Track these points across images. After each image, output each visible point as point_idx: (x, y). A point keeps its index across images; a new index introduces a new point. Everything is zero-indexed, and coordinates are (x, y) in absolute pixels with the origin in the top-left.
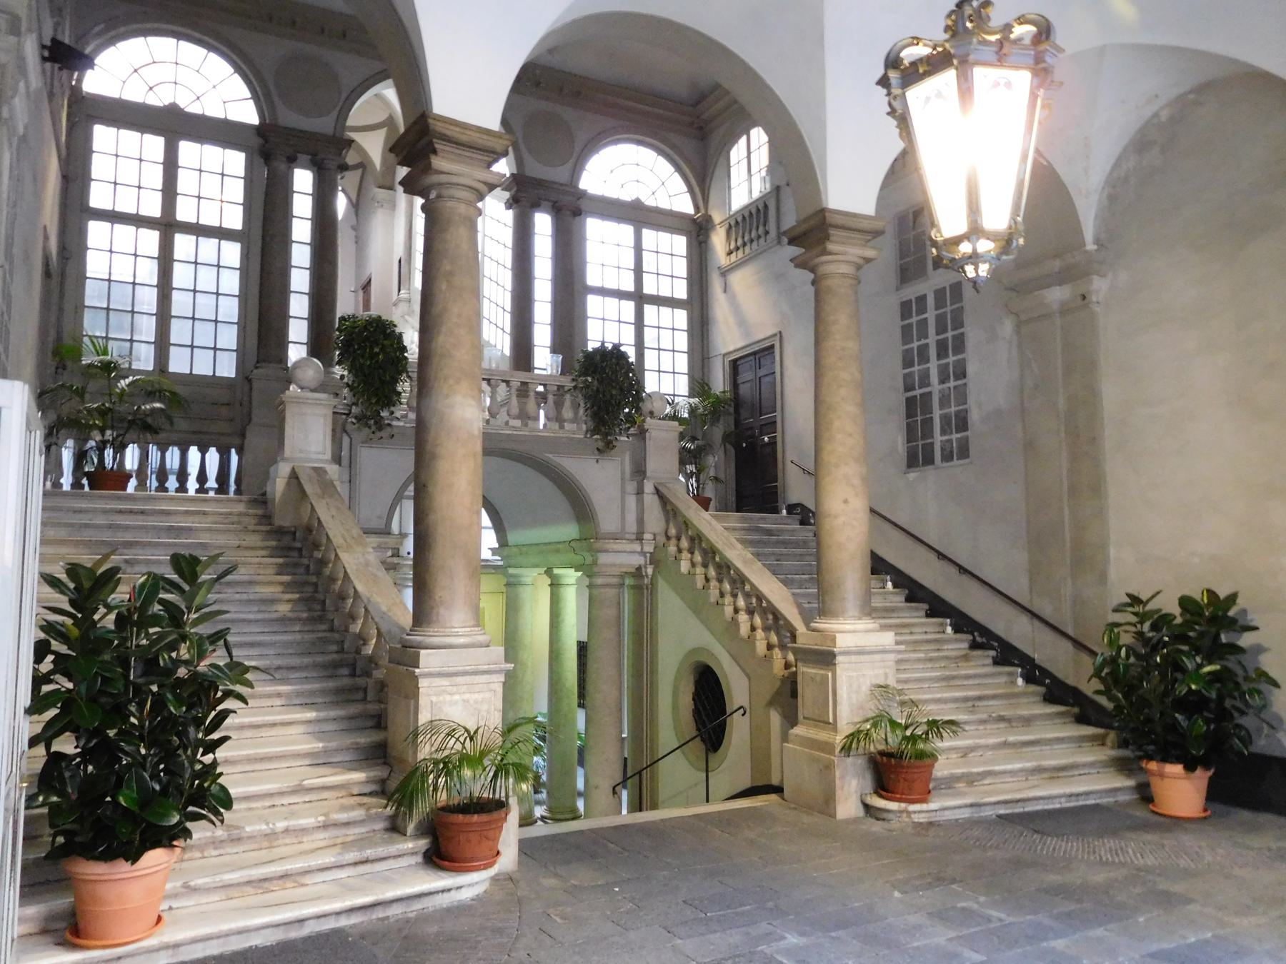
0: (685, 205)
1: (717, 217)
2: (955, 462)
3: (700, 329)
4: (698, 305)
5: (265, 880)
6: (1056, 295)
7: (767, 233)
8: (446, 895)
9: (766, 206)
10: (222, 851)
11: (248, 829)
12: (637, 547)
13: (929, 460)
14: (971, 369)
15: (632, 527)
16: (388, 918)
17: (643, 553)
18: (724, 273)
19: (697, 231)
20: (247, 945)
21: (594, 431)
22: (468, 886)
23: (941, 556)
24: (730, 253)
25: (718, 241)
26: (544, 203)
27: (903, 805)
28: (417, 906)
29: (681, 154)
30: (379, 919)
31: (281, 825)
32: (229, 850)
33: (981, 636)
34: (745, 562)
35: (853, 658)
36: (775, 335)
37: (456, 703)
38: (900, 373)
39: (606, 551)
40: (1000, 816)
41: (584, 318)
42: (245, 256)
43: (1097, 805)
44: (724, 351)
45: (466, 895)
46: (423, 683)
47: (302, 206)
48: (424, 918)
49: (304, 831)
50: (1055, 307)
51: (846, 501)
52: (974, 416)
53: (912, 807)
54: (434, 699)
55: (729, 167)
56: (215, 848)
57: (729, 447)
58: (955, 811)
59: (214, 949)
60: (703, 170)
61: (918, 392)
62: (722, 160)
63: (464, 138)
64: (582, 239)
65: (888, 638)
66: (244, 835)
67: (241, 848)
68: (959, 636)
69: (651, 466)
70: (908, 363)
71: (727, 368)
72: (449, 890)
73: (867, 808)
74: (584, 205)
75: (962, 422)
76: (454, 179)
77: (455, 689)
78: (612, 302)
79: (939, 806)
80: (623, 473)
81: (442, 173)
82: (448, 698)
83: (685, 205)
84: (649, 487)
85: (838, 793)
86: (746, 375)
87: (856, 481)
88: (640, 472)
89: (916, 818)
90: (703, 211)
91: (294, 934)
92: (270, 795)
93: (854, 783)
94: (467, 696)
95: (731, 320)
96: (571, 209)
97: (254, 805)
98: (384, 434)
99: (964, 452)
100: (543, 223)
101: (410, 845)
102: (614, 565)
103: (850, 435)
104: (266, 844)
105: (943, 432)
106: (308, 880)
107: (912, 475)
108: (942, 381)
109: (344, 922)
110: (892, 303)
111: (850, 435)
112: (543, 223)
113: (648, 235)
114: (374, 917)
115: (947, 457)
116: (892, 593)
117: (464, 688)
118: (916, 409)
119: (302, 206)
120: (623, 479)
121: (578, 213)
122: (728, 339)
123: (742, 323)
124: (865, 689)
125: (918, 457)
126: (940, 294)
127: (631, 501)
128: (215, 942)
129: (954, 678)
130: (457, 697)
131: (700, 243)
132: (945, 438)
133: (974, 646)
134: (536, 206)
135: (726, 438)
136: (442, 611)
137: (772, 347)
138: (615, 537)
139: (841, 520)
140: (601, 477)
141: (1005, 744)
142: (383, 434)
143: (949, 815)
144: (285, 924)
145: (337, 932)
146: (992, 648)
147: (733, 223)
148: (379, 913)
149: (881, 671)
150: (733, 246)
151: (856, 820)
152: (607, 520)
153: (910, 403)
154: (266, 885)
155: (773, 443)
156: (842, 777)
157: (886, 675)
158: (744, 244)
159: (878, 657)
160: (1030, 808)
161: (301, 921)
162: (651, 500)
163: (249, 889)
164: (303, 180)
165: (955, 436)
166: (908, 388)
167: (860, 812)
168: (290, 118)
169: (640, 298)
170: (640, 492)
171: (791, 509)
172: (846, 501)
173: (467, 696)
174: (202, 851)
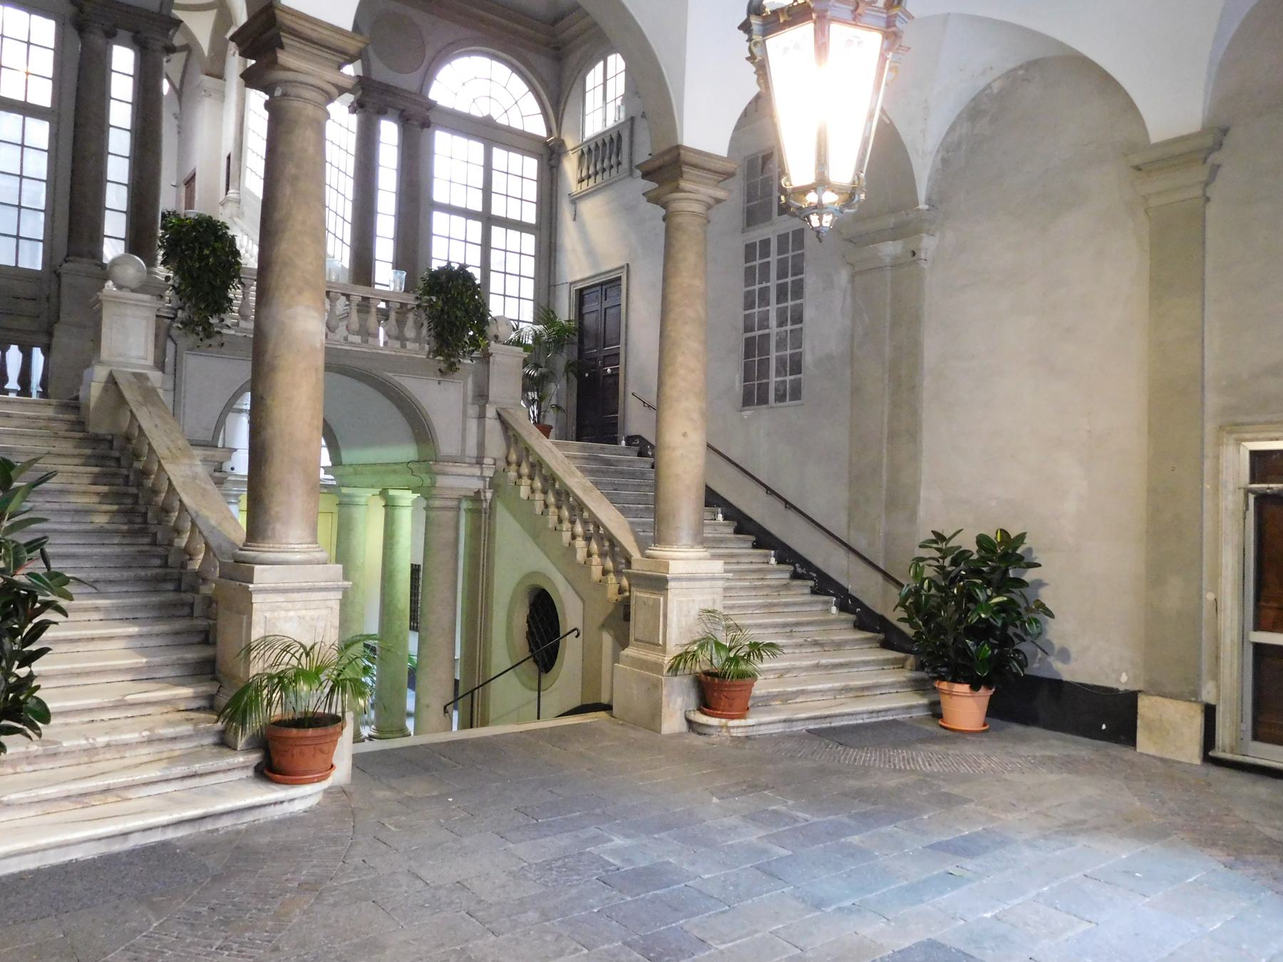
0: (537, 126)
1: (570, 143)
2: (788, 402)
3: (548, 256)
4: (547, 231)
5: (86, 794)
6: (890, 249)
7: (619, 163)
8: (278, 807)
9: (619, 136)
10: (36, 767)
11: (65, 744)
12: (477, 471)
13: (763, 400)
14: (808, 314)
15: (472, 450)
16: (217, 830)
17: (483, 478)
18: (575, 200)
19: (549, 155)
20: (67, 858)
21: (437, 352)
22: (301, 798)
23: (769, 491)
24: (581, 181)
25: (570, 167)
26: (122, 33)
27: (724, 721)
28: (249, 817)
29: (546, 88)
30: (208, 831)
31: (102, 740)
32: (44, 766)
33: (802, 567)
34: (585, 490)
35: (684, 584)
36: (622, 267)
37: (291, 619)
38: (741, 313)
39: (445, 474)
40: (808, 731)
41: (429, 234)
42: (54, 136)
43: (894, 721)
44: (570, 280)
45: (298, 807)
46: (256, 598)
47: (122, 87)
48: (256, 829)
49: (127, 745)
50: (888, 260)
51: (685, 435)
52: (808, 359)
53: (731, 723)
54: (268, 615)
55: (584, 92)
56: (30, 764)
57: (572, 376)
58: (770, 726)
59: (29, 864)
60: (558, 93)
61: (757, 333)
62: (578, 80)
63: (314, 35)
64: (431, 153)
65: (718, 566)
66: (61, 750)
67: (58, 764)
68: (782, 566)
69: (495, 390)
70: (749, 304)
71: (573, 296)
72: (282, 802)
73: (690, 723)
74: (433, 117)
75: (796, 365)
76: (301, 78)
77: (290, 605)
78: (459, 221)
79: (758, 722)
80: (465, 394)
81: (289, 70)
82: (283, 614)
83: (537, 126)
84: (491, 412)
85: (664, 710)
86: (591, 306)
87: (696, 416)
88: (482, 396)
89: (735, 733)
90: (556, 135)
91: (117, 847)
92: (91, 710)
93: (679, 701)
94: (303, 613)
95: (579, 248)
96: (419, 120)
97: (70, 720)
98: (214, 341)
99: (796, 393)
100: (389, 131)
101: (241, 759)
102: (452, 488)
103: (693, 371)
104: (86, 759)
105: (778, 373)
106: (131, 794)
107: (747, 413)
108: (781, 324)
109: (171, 835)
110: (737, 245)
111: (693, 371)
112: (389, 131)
113: (499, 155)
114: (203, 829)
115: (781, 397)
116: (720, 525)
117: (299, 605)
118: (754, 349)
119: (122, 87)
120: (465, 404)
121: (426, 124)
122: (576, 267)
123: (591, 252)
124: (695, 611)
125: (754, 396)
126: (782, 239)
127: (473, 425)
128: (30, 856)
129: (774, 605)
130: (292, 613)
131: (552, 168)
132: (779, 379)
133: (795, 576)
134: (382, 112)
135: (569, 366)
136: (278, 526)
137: (619, 279)
138: (454, 460)
139: (678, 453)
140: (443, 400)
141: (818, 666)
142: (208, 342)
143: (764, 730)
144: (100, 839)
145: (164, 844)
146: (811, 579)
147: (585, 150)
148: (209, 826)
149: (709, 597)
150: (584, 174)
151: (680, 735)
152: (447, 444)
153: (749, 343)
154: (87, 800)
155: (615, 375)
156: (669, 695)
157: (714, 601)
158: (596, 173)
159: (707, 583)
160: (837, 723)
161: (125, 834)
162: (492, 425)
163: (67, 804)
164: (123, 58)
165: (789, 378)
166: (748, 328)
167: (684, 728)
168: (382, 73)
169: (488, 219)
170: (482, 416)
171: (630, 440)
172: (685, 435)
173: (303, 613)
174: (14, 766)
